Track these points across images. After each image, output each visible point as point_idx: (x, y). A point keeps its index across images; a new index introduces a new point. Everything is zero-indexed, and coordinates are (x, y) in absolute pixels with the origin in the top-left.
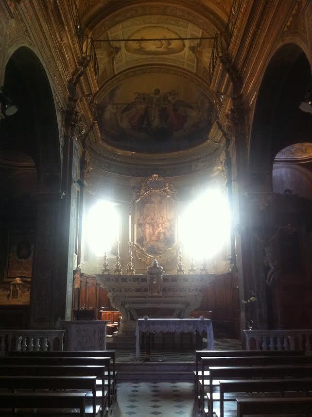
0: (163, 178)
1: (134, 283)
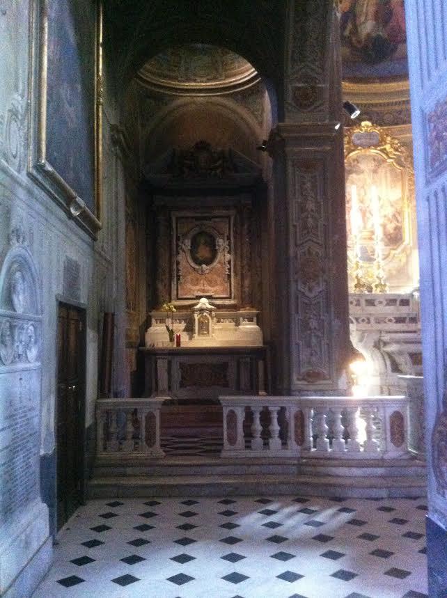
0: (379, 128)
1: (388, 307)
